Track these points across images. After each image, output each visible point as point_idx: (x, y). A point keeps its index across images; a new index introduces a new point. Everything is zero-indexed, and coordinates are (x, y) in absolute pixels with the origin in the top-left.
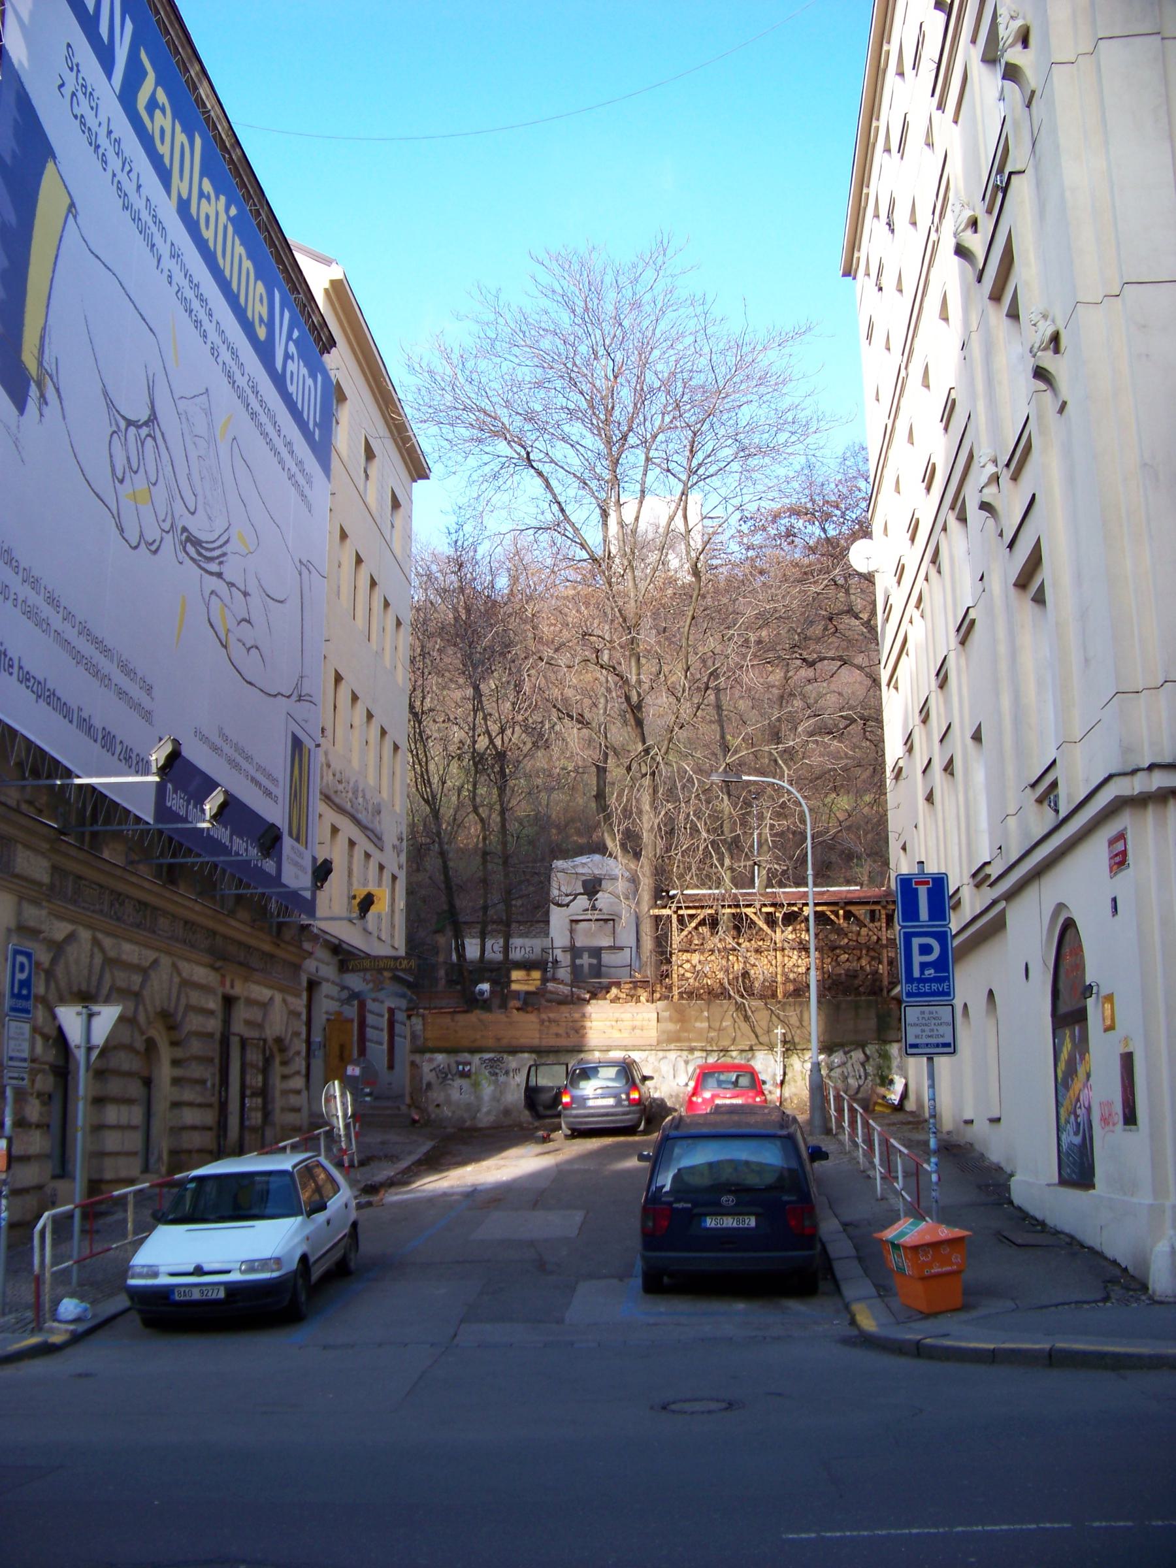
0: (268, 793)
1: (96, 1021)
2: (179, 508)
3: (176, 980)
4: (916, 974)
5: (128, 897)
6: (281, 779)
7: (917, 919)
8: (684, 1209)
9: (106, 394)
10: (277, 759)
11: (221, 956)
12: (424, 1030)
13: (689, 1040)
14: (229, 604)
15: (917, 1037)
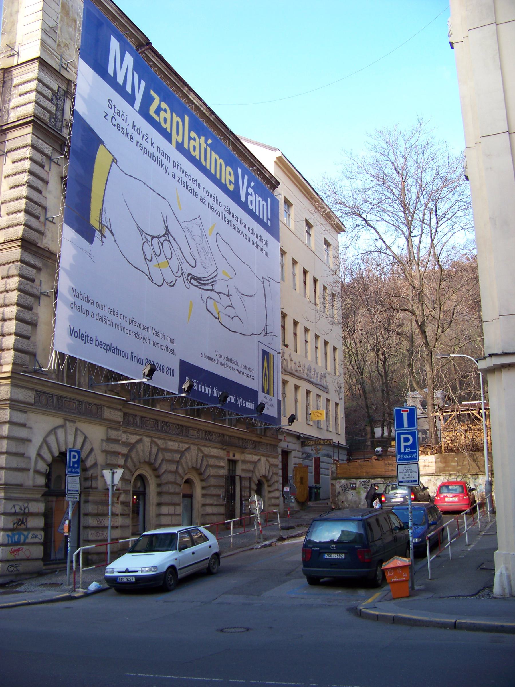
0: (247, 375)
1: (115, 475)
2: (185, 266)
3: (201, 455)
4: (402, 451)
5: (171, 423)
6: (256, 370)
7: (403, 427)
8: (316, 550)
9: (139, 228)
10: (254, 362)
11: (226, 442)
12: (337, 470)
13: (449, 471)
14: (219, 300)
15: (403, 478)
